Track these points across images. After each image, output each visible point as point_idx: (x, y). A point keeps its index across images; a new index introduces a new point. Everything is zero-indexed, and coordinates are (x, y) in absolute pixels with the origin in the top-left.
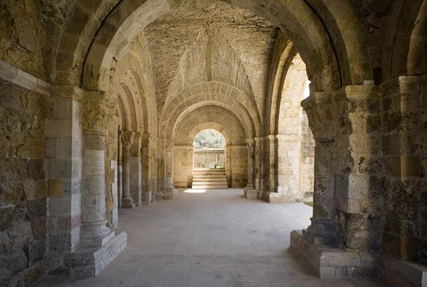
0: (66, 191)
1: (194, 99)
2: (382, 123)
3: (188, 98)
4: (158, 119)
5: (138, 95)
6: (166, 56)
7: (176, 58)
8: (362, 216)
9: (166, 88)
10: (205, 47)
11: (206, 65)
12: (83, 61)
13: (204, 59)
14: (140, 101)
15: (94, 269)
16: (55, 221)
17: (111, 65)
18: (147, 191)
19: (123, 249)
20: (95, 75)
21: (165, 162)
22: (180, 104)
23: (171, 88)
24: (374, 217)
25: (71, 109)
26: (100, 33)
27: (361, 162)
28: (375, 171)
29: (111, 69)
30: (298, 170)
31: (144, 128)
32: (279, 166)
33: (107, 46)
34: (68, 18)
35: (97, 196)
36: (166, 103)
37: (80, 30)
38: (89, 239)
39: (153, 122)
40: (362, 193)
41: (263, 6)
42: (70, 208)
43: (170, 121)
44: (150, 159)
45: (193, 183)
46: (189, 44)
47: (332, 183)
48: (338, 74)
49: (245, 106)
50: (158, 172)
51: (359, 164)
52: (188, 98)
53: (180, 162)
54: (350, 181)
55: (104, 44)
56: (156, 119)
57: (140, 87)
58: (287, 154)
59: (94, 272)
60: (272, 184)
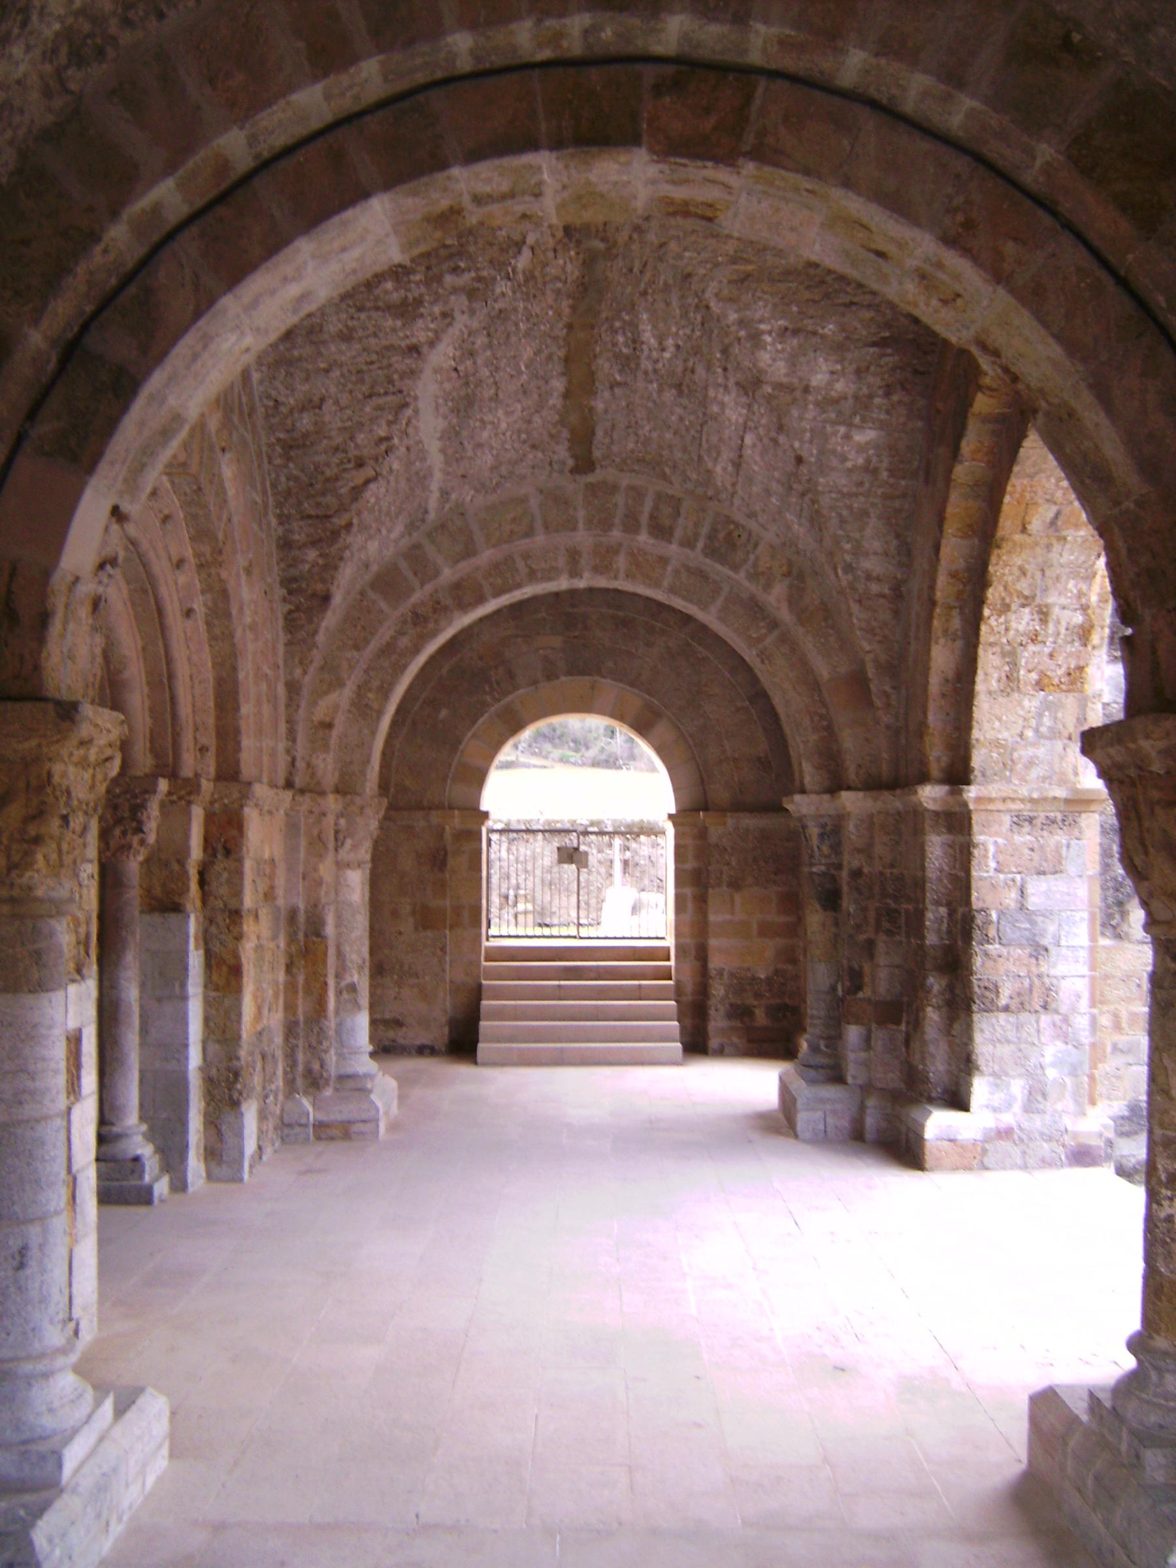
1: (496, 567)
3: (465, 567)
4: (293, 688)
5: (188, 577)
6: (347, 353)
7: (400, 363)
9: (339, 521)
10: (565, 304)
11: (566, 395)
13: (558, 368)
14: (199, 605)
17: (104, 543)
18: (235, 1104)
19: (151, 1480)
21: (330, 930)
22: (417, 597)
29: (101, 566)
30: (1082, 986)
31: (220, 751)
32: (978, 962)
33: (91, 468)
36: (337, 599)
39: (266, 710)
41: (880, 254)
43: (361, 689)
44: (249, 926)
46: (471, 294)
49: (785, 615)
50: (291, 987)
52: (465, 567)
56: (281, 690)
57: (202, 534)
58: (1022, 892)
60: (937, 1067)
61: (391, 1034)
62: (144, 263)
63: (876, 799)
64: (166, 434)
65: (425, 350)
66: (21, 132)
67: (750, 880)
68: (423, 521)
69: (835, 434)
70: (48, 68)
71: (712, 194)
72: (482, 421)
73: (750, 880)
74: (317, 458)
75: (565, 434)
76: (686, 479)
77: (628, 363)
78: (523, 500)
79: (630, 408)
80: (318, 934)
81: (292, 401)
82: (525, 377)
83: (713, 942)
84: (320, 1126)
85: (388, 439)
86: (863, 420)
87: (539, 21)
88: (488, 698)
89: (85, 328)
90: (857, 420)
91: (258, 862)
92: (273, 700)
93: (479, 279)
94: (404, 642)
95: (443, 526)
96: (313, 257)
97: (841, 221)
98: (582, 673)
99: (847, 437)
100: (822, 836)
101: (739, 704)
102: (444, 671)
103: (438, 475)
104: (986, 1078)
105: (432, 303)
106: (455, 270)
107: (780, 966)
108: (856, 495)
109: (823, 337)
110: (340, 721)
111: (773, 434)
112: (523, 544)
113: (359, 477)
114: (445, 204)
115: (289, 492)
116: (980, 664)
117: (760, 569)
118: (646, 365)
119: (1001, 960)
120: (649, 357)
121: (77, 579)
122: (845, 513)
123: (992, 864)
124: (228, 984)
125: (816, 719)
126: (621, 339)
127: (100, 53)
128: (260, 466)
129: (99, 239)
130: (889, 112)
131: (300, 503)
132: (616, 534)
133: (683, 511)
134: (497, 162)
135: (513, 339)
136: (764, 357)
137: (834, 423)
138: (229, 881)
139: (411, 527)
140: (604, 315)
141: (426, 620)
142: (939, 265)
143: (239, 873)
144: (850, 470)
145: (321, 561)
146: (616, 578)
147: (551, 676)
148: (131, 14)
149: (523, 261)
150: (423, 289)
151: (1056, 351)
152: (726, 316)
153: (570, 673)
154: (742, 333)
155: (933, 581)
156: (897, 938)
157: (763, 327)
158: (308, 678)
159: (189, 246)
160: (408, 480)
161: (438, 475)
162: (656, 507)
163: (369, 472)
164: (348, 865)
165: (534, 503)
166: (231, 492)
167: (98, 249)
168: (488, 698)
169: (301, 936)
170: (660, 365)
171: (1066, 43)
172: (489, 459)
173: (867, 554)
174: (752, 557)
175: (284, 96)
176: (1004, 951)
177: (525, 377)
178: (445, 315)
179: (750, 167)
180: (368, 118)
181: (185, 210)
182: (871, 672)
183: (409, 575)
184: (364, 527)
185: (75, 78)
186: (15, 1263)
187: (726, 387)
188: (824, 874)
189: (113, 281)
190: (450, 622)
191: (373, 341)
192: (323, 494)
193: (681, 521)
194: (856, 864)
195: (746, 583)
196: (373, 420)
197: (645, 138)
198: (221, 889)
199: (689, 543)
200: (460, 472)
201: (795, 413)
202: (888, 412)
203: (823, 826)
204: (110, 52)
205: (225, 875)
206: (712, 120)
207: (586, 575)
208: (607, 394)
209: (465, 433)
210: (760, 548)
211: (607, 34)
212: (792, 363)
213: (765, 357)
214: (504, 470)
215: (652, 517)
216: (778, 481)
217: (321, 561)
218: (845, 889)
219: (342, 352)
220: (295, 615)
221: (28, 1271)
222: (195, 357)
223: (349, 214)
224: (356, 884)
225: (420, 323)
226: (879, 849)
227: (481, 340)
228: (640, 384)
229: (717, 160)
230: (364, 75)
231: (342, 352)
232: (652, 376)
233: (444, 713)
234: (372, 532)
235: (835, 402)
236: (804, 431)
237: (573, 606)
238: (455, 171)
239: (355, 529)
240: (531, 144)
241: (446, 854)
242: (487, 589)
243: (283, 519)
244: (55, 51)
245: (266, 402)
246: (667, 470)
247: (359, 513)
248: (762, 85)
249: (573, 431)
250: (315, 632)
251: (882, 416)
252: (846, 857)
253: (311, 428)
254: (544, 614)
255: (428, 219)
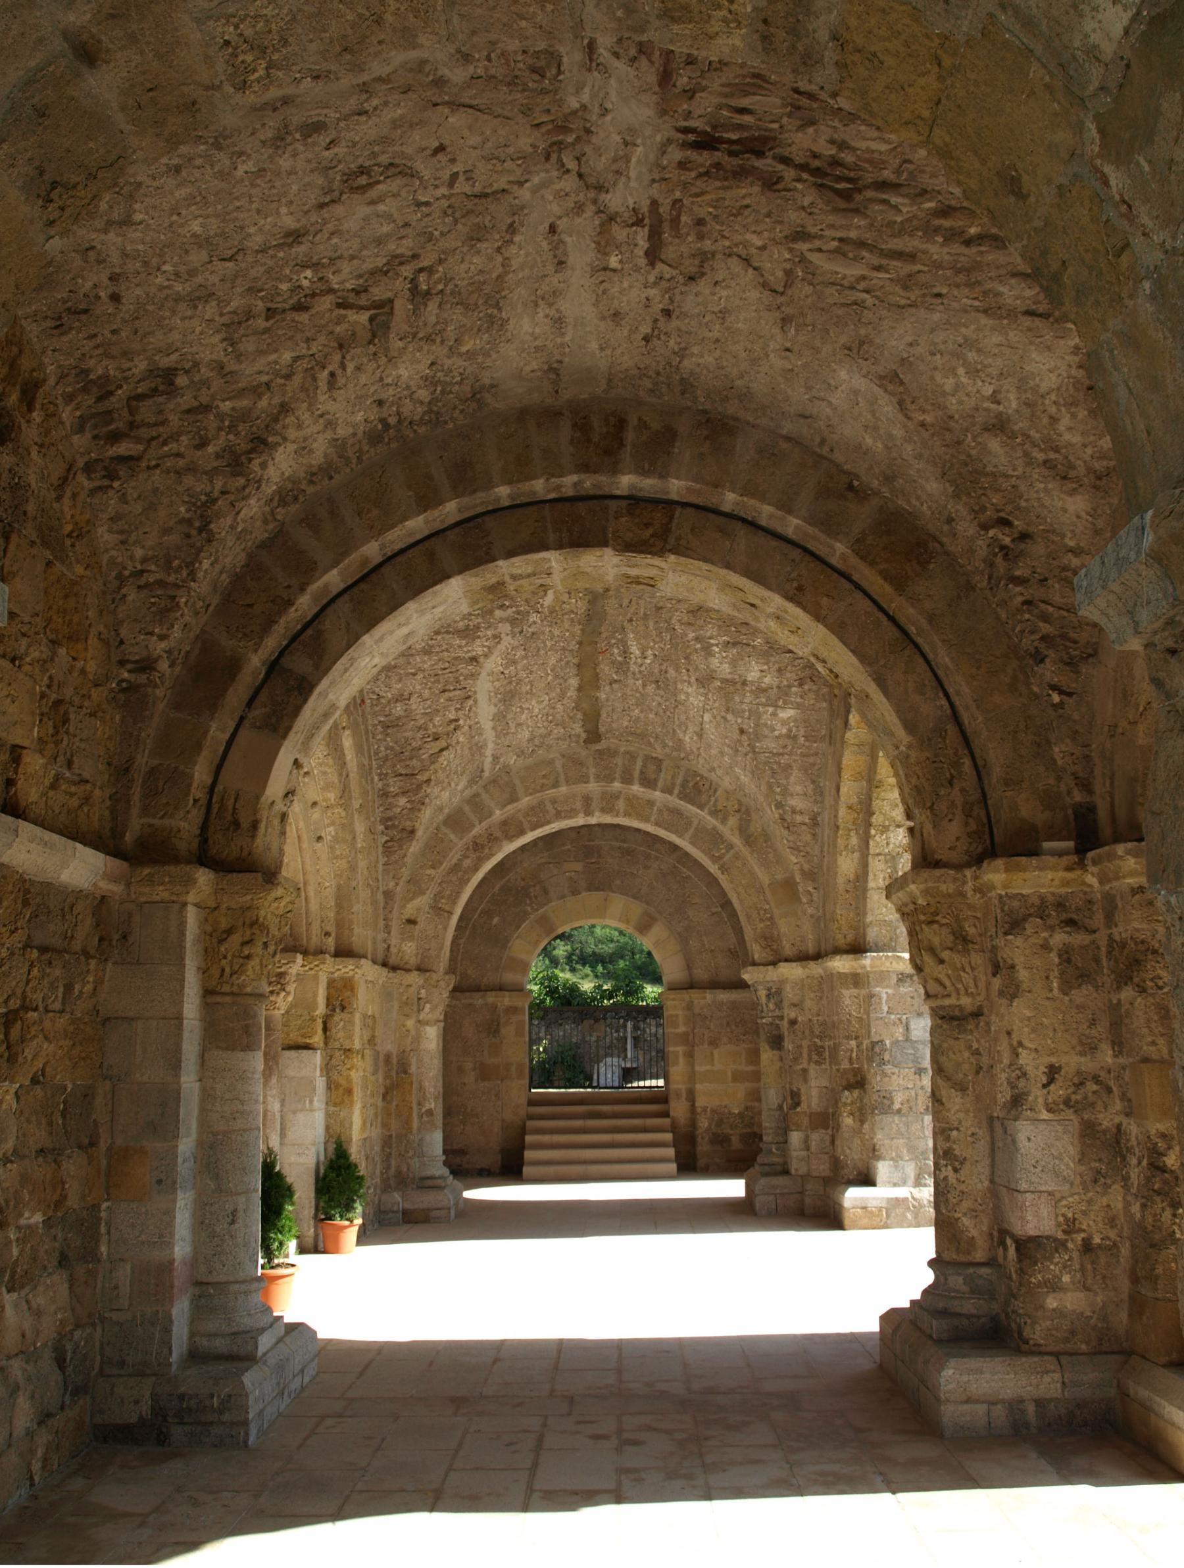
0: (159, 1182)
2: (1104, 962)
4: (388, 895)
6: (428, 663)
7: (465, 669)
8: (1063, 1244)
10: (577, 629)
11: (580, 689)
12: (209, 781)
13: (574, 671)
15: (245, 1423)
16: (124, 1274)
17: (289, 781)
20: (245, 824)
21: (413, 1069)
22: (476, 831)
23: (441, 775)
24: (1099, 1246)
25: (182, 934)
26: (263, 697)
27: (1051, 1081)
28: (1093, 1104)
29: (286, 795)
34: (178, 669)
35: (242, 1200)
37: (213, 704)
38: (215, 1335)
40: (1057, 1174)
41: (753, 605)
42: (172, 1234)
43: (437, 896)
45: (529, 1155)
46: (513, 622)
47: (983, 1145)
48: (983, 813)
51: (1045, 1086)
53: (469, 1066)
54: (1021, 1137)
55: (275, 730)
58: (907, 1028)
59: (247, 1434)
61: (458, 1160)
62: (317, 616)
63: (804, 967)
64: (326, 716)
65: (481, 660)
66: (250, 544)
67: (725, 1040)
68: (481, 777)
69: (765, 713)
70: (267, 509)
71: (653, 572)
72: (521, 707)
73: (725, 1040)
74: (407, 734)
75: (580, 716)
76: (665, 746)
77: (622, 667)
78: (551, 762)
79: (624, 698)
80: (406, 1072)
81: (389, 695)
82: (550, 678)
83: (698, 1087)
84: (405, 1213)
85: (456, 720)
86: (785, 703)
87: (547, 479)
88: (529, 909)
89: (281, 654)
90: (781, 703)
91: (365, 1016)
92: (374, 902)
93: (518, 613)
94: (467, 863)
95: (494, 781)
96: (417, 612)
97: (725, 587)
98: (598, 889)
99: (774, 715)
100: (768, 996)
101: (714, 910)
102: (496, 889)
103: (491, 745)
104: (887, 1163)
105: (487, 628)
106: (502, 607)
107: (749, 1104)
108: (782, 754)
109: (753, 647)
110: (422, 920)
111: (723, 714)
112: (552, 792)
113: (435, 747)
114: (494, 580)
115: (386, 758)
116: (870, 869)
117: (719, 808)
118: (633, 668)
119: (895, 1077)
120: (635, 663)
121: (273, 802)
122: (775, 767)
123: (886, 1009)
124: (343, 1101)
125: (762, 912)
126: (616, 651)
127: (296, 498)
128: (367, 740)
129: (293, 604)
130: (753, 525)
131: (395, 766)
132: (617, 785)
133: (663, 767)
134: (525, 557)
135: (542, 652)
136: (715, 662)
137: (764, 705)
138: (344, 1028)
139: (472, 782)
140: (604, 636)
141: (483, 847)
142: (786, 612)
143: (352, 1022)
144: (777, 737)
145: (409, 806)
146: (617, 816)
147: (575, 892)
148: (314, 478)
149: (549, 599)
150: (480, 620)
151: (854, 659)
152: (686, 635)
153: (589, 889)
154: (698, 646)
155: (837, 811)
156: (823, 1066)
157: (712, 641)
158: (398, 888)
159: (343, 605)
160: (470, 749)
161: (491, 745)
162: (644, 766)
163: (442, 743)
164: (427, 1023)
165: (559, 764)
166: (349, 757)
167: (293, 609)
168: (529, 909)
169: (394, 1074)
170: (643, 668)
171: (850, 487)
172: (526, 734)
173: (792, 795)
174: (713, 799)
175: (401, 522)
176: (896, 1070)
177: (550, 678)
178: (495, 637)
179: (672, 558)
180: (448, 533)
181: (342, 586)
182: (798, 878)
183: (471, 815)
184: (439, 782)
185: (281, 513)
186: (229, 1220)
187: (689, 683)
188: (771, 1024)
189: (299, 627)
190: (500, 849)
191: (446, 654)
192: (411, 759)
193: (662, 775)
194: (793, 1015)
195: (709, 818)
196: (446, 708)
197: (611, 542)
198: (338, 1032)
199: (668, 790)
200: (506, 743)
201: (737, 699)
202: (802, 697)
203: (769, 989)
204: (301, 498)
205: (342, 1023)
206: (650, 531)
207: (597, 814)
208: (607, 688)
209: (509, 716)
210: (718, 793)
211: (588, 484)
212: (734, 664)
213: (715, 662)
214: (537, 742)
215: (642, 773)
216: (729, 746)
217: (409, 806)
218: (786, 1033)
219: (424, 662)
220: (390, 844)
221: (237, 1226)
222: (346, 670)
223: (438, 587)
224: (432, 1037)
225: (478, 642)
226: (808, 1003)
227: (520, 653)
228: (631, 682)
229: (653, 554)
230: (447, 510)
231: (424, 662)
232: (638, 676)
233: (496, 920)
234: (445, 785)
235: (765, 690)
236: (744, 711)
237: (589, 841)
238: (500, 563)
239: (433, 783)
240: (545, 547)
241: (498, 1025)
242: (526, 825)
243: (383, 776)
244: (271, 500)
245: (371, 696)
246: (652, 740)
247: (436, 772)
248: (678, 511)
249: (585, 714)
250: (405, 856)
251: (799, 700)
252: (786, 1011)
253: (402, 713)
254: (569, 847)
255: (483, 588)
